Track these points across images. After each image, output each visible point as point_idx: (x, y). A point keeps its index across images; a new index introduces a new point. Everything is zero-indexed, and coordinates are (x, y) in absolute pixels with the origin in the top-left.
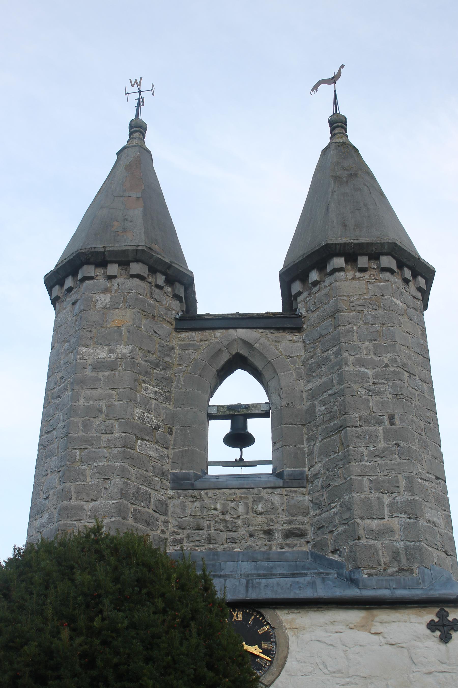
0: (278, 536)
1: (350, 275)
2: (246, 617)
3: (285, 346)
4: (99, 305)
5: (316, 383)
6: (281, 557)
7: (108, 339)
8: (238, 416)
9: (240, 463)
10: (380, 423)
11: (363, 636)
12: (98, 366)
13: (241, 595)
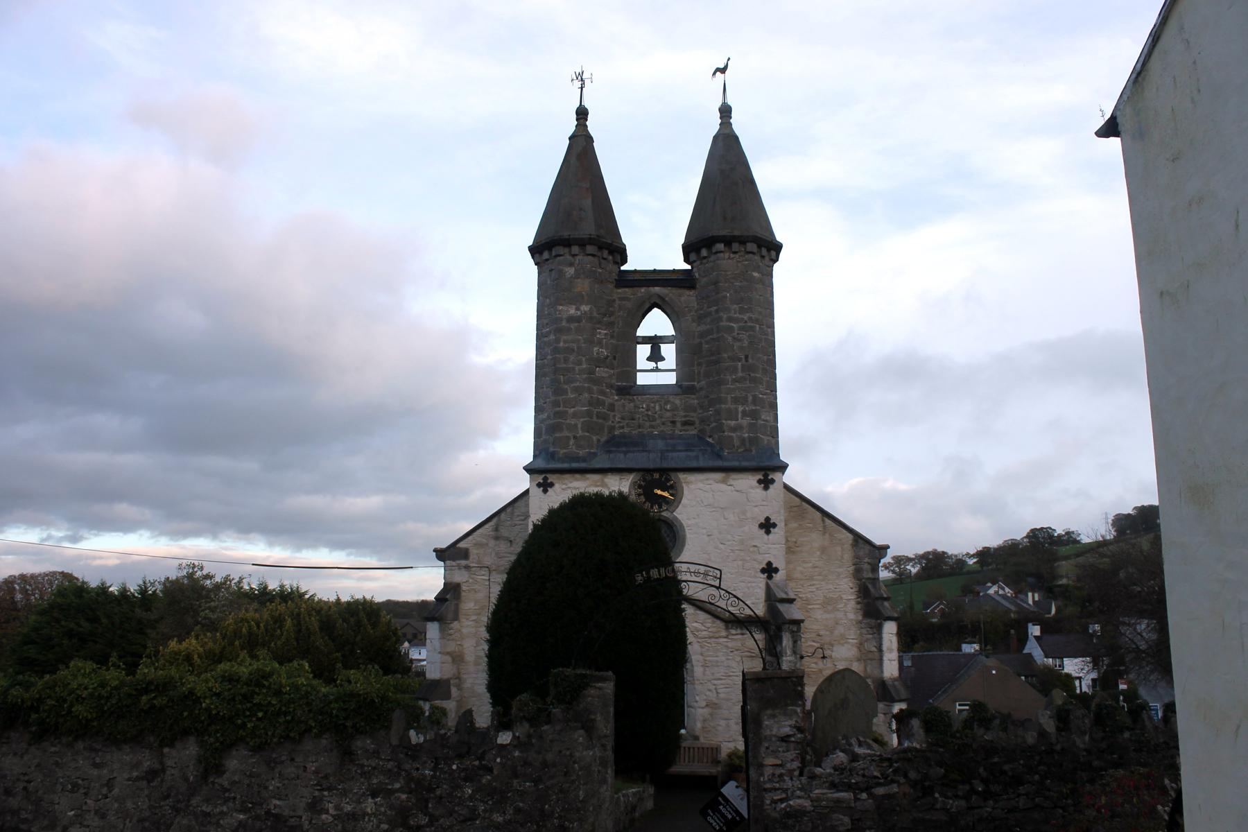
0: (679, 425)
1: (727, 255)
2: (661, 476)
3: (687, 298)
4: (568, 275)
5: (703, 328)
6: (680, 437)
7: (577, 300)
8: (655, 342)
9: (657, 370)
10: (740, 360)
11: (723, 486)
12: (571, 319)
13: (658, 465)
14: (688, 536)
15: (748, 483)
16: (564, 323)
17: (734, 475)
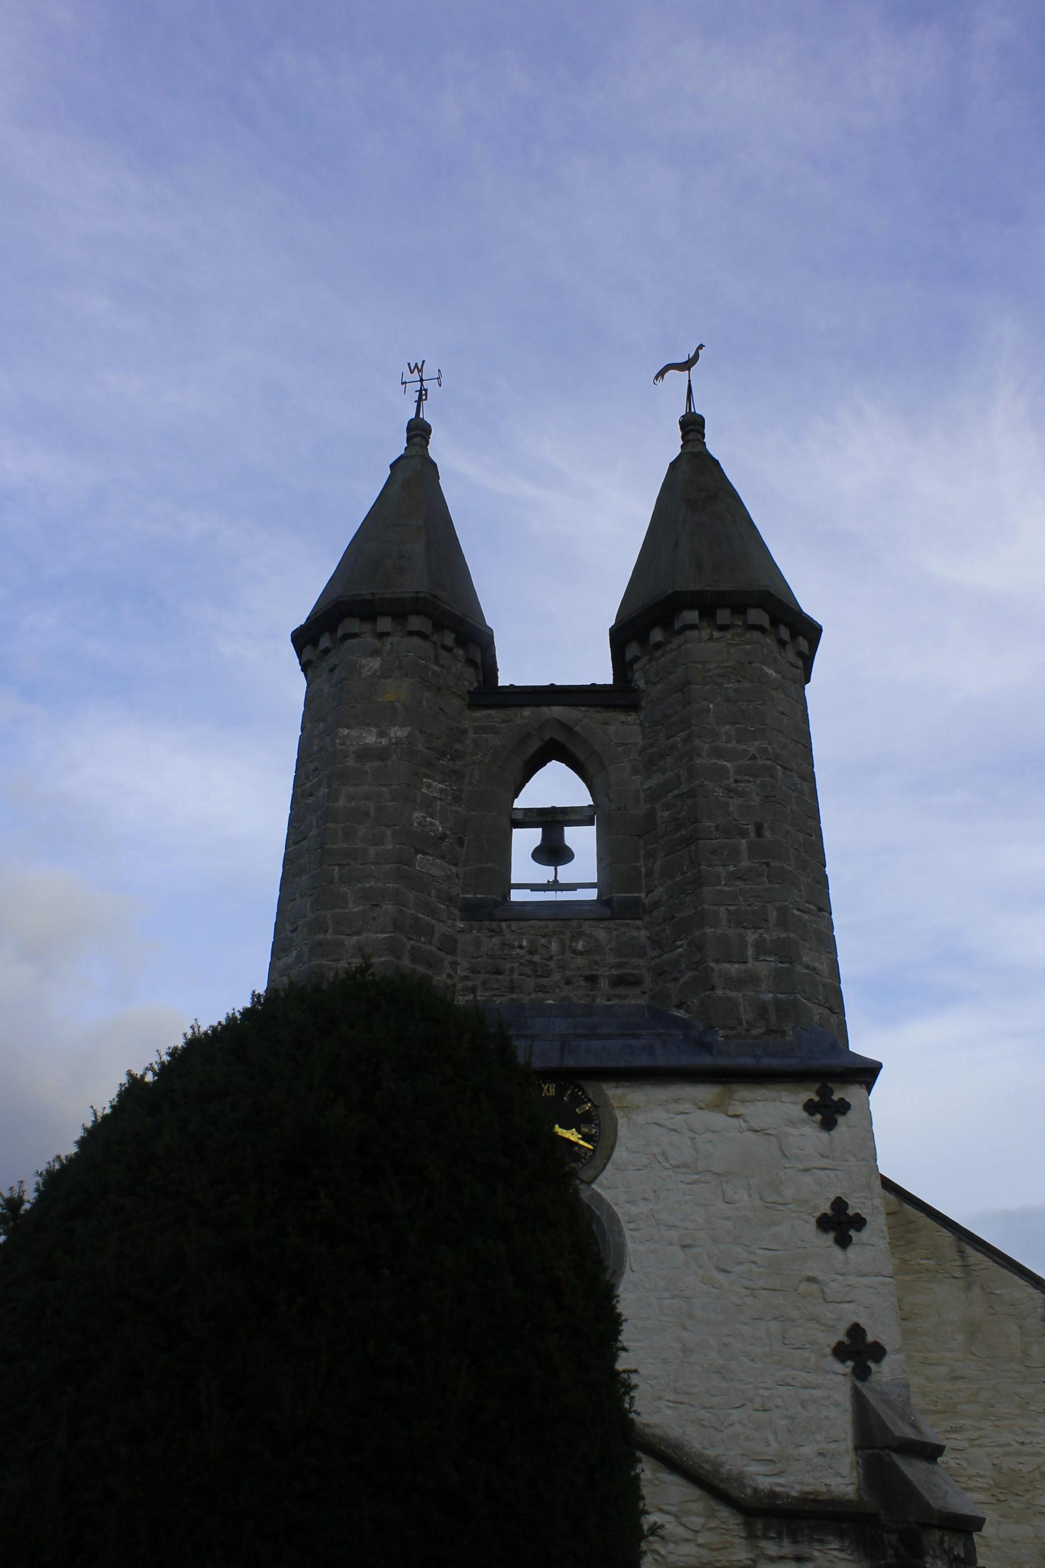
0: (604, 985)
1: (705, 634)
3: (621, 728)
4: (366, 672)
5: (657, 779)
8: (552, 821)
9: (554, 886)
10: (743, 833)
11: (717, 1119)
12: (365, 754)
13: (554, 1061)
14: (630, 1246)
15: (781, 1109)
16: (351, 762)
17: (744, 1092)
